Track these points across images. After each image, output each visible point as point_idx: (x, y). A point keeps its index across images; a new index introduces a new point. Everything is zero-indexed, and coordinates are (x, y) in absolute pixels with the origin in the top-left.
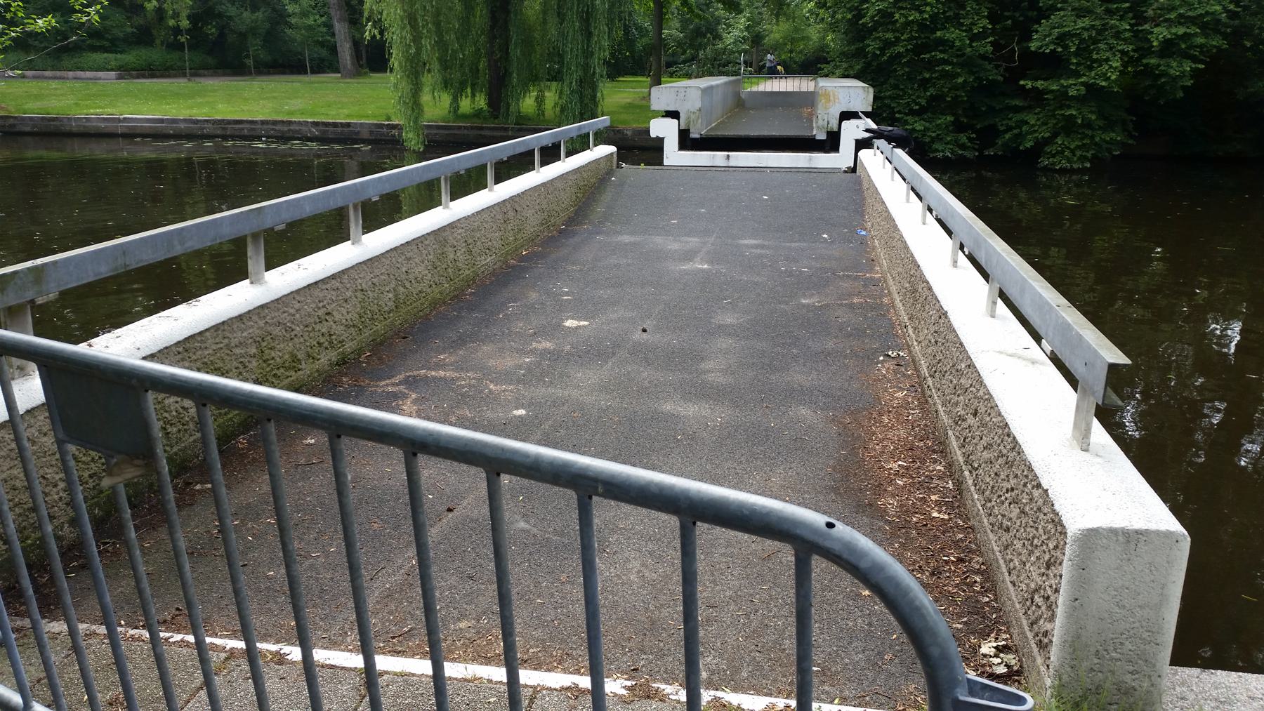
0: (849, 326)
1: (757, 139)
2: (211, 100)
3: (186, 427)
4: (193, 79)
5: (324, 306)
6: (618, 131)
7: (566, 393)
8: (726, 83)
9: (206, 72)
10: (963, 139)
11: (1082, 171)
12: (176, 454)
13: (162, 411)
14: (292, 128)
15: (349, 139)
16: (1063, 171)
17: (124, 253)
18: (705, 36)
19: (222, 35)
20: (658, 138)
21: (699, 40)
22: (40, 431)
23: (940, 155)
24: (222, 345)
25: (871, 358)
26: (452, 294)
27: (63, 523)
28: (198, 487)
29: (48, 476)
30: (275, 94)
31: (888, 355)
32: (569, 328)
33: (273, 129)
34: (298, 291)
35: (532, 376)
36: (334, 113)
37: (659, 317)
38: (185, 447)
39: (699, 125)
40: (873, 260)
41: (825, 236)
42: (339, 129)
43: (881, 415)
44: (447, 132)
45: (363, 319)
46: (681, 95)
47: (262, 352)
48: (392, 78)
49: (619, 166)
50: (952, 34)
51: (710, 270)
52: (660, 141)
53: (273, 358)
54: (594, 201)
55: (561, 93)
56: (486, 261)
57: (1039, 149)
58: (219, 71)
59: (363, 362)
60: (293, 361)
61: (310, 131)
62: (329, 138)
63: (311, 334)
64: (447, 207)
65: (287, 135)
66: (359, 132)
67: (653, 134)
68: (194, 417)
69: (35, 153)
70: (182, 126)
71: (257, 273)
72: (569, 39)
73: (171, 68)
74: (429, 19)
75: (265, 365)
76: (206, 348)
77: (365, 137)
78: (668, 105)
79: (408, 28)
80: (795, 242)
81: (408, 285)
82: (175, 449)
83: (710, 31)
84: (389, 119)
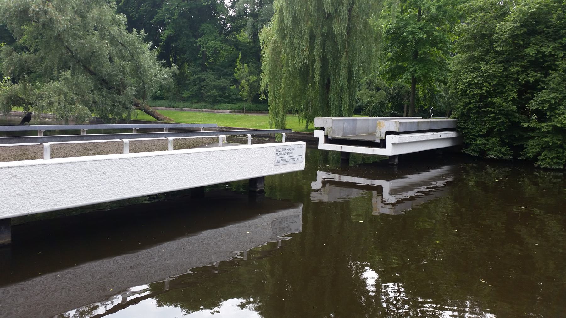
4: (246, 114)
8: (453, 121)
10: (503, 150)
11: (559, 170)
16: (546, 169)
23: (489, 157)
50: (498, 100)
52: (317, 139)
57: (535, 158)
73: (252, 110)
78: (320, 125)
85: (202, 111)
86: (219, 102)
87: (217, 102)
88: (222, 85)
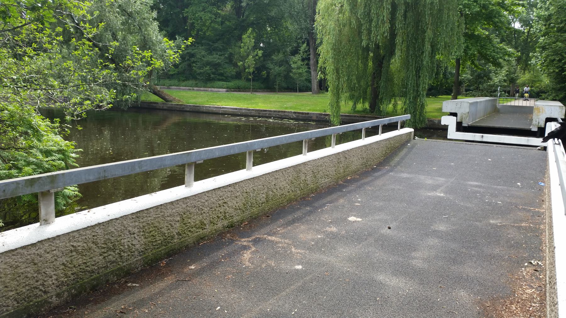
0: (513, 240)
1: (485, 127)
2: (257, 101)
3: (133, 254)
4: (253, 93)
5: (223, 199)
6: (431, 120)
7: (329, 259)
8: (486, 101)
9: (260, 90)
12: (124, 266)
13: (119, 246)
14: (285, 114)
15: (307, 119)
17: (105, 171)
18: (482, 78)
19: (268, 76)
20: (445, 125)
21: (480, 80)
22: (45, 251)
24: (159, 216)
25: (519, 263)
26: (301, 196)
27: (52, 295)
28: (129, 285)
29: (47, 273)
30: (282, 100)
31: (531, 263)
32: (350, 221)
33: (278, 114)
34: (208, 192)
35: (318, 246)
36: (303, 108)
37: (402, 221)
38: (131, 263)
39: (467, 120)
40: (543, 201)
41: (519, 184)
42: (304, 115)
43: (512, 303)
44: (350, 118)
45: (246, 206)
46: (459, 106)
47: (183, 220)
48: (329, 94)
49: (414, 139)
51: (443, 197)
53: (189, 223)
54: (395, 155)
55: (405, 102)
56: (324, 181)
58: (265, 90)
59: (242, 227)
60: (202, 224)
61: (292, 115)
62: (299, 119)
63: (213, 212)
64: (305, 154)
65: (283, 117)
66: (312, 117)
67: (443, 123)
68: (138, 249)
69: (191, 119)
70: (244, 111)
71: (189, 182)
72: (410, 79)
74: (344, 70)
75: (184, 226)
76: (150, 216)
77: (314, 119)
78: (451, 110)
79: (335, 74)
80: (500, 186)
81: (275, 191)
82: (125, 264)
83: (486, 76)
84: (325, 111)
85: (193, 90)
86: (213, 80)
87: (211, 80)
88: (216, 61)
